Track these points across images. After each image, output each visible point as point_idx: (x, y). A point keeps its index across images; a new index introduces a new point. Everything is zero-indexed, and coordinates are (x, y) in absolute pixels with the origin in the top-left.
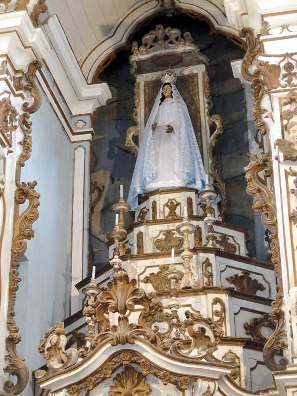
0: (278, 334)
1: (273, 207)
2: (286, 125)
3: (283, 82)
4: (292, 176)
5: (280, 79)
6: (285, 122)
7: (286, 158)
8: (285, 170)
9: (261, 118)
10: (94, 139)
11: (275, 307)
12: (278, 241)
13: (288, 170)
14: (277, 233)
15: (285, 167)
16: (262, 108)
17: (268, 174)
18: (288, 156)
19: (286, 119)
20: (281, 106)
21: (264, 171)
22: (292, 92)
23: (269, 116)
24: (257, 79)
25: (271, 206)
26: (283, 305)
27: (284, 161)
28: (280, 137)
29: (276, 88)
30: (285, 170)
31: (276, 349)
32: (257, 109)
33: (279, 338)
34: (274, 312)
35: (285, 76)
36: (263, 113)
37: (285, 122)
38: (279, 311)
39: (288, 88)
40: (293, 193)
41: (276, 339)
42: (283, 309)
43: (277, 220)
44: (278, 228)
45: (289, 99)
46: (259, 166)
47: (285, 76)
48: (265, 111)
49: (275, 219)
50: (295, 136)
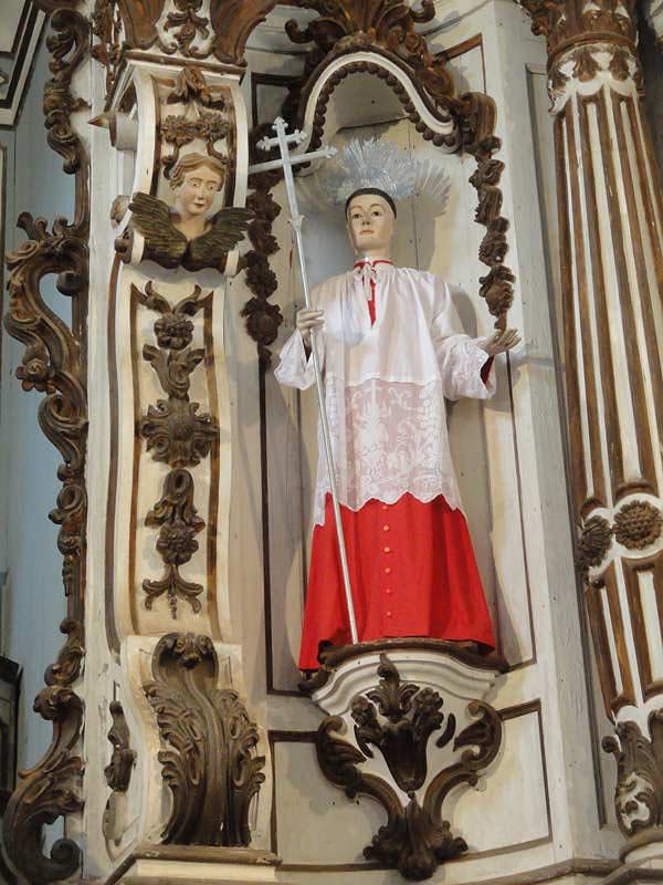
0: (60, 766)
1: (78, 385)
2: (170, 158)
3: (168, 37)
4: (149, 308)
5: (160, 25)
6: (168, 150)
7: (149, 254)
8: (133, 287)
9: (69, 122)
10: (479, 48)
11: (57, 682)
12: (84, 488)
13: (142, 289)
14: (83, 461)
15: (130, 278)
16: (76, 97)
17: (74, 288)
18: (158, 249)
19: (172, 141)
20: (159, 101)
21: (64, 274)
22: (192, 71)
23: (106, 122)
24: (69, 9)
25: (74, 381)
26: (79, 680)
27: (143, 258)
28: (147, 191)
29: (144, 48)
30: (133, 287)
31: (50, 810)
32: (61, 94)
33: (62, 779)
34: (53, 698)
35: (173, 21)
36: (76, 110)
37: (168, 150)
38: (69, 697)
39: (178, 56)
40: (148, 357)
41: (52, 780)
42: (79, 690)
43: (87, 424)
44: (89, 448)
45: (185, 88)
46: (49, 256)
47: (173, 21)
48: (83, 105)
49: (83, 421)
50: (194, 197)
